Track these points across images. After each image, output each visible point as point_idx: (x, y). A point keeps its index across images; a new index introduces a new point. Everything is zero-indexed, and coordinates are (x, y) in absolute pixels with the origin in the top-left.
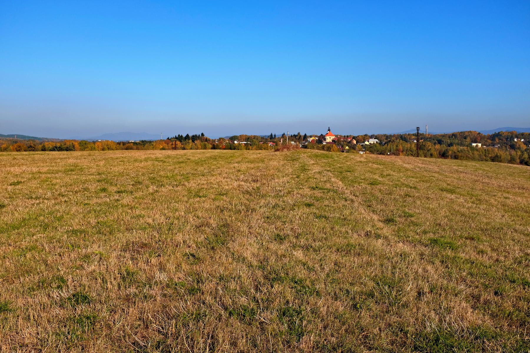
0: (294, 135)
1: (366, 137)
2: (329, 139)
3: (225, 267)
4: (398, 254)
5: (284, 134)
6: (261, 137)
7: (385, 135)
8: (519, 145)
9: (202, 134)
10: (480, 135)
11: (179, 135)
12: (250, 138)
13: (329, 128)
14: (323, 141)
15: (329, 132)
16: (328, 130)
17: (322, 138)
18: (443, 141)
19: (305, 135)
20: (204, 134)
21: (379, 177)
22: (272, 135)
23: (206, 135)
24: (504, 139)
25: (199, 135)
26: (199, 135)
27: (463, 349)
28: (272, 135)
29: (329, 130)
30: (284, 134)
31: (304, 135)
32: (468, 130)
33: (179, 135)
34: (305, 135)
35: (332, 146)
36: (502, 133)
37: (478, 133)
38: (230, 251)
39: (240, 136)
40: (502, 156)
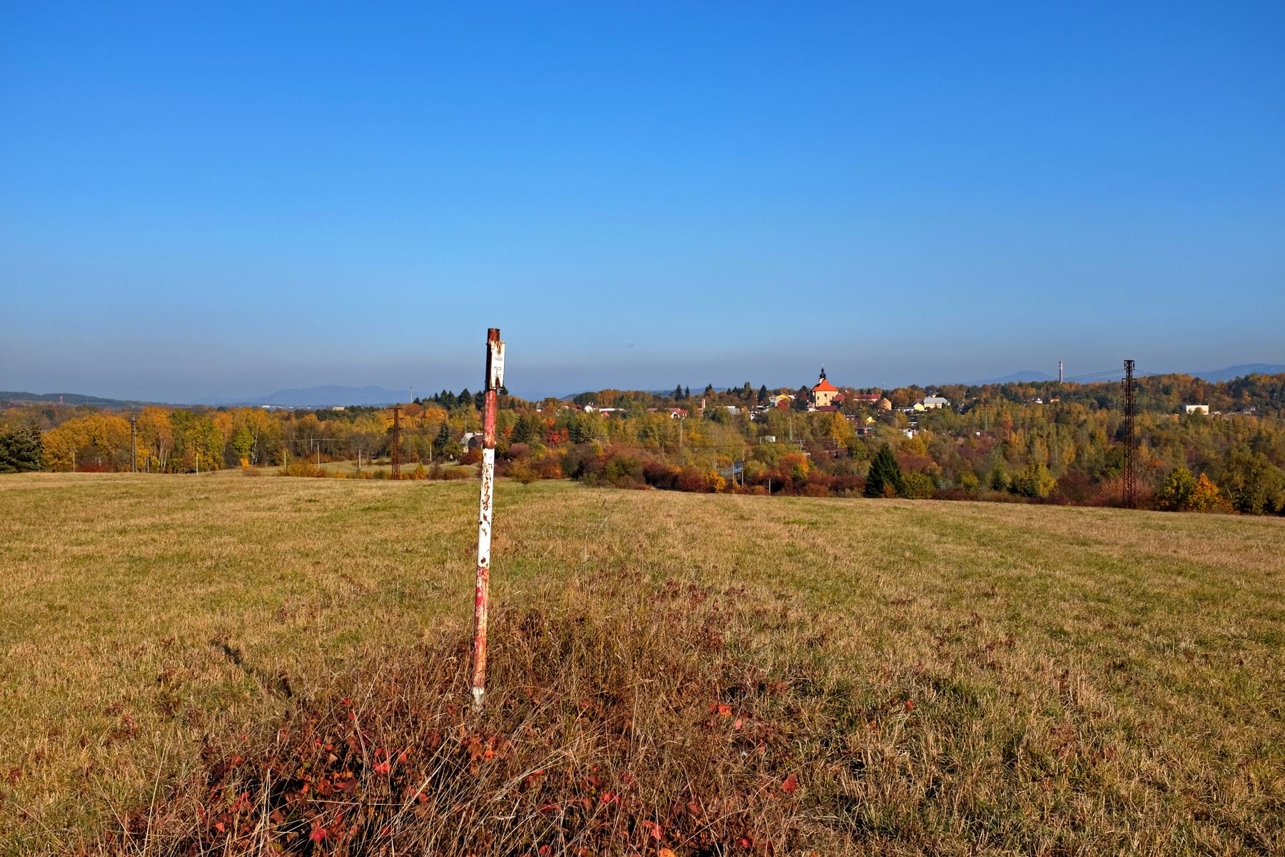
1: (915, 394)
5: (710, 387)
11: (444, 393)
13: (822, 370)
14: (807, 404)
15: (821, 380)
16: (821, 377)
17: (804, 397)
19: (764, 388)
22: (679, 390)
28: (679, 390)
29: (823, 376)
30: (710, 387)
33: (444, 393)
34: (764, 388)
35: (834, 416)
39: (602, 392)
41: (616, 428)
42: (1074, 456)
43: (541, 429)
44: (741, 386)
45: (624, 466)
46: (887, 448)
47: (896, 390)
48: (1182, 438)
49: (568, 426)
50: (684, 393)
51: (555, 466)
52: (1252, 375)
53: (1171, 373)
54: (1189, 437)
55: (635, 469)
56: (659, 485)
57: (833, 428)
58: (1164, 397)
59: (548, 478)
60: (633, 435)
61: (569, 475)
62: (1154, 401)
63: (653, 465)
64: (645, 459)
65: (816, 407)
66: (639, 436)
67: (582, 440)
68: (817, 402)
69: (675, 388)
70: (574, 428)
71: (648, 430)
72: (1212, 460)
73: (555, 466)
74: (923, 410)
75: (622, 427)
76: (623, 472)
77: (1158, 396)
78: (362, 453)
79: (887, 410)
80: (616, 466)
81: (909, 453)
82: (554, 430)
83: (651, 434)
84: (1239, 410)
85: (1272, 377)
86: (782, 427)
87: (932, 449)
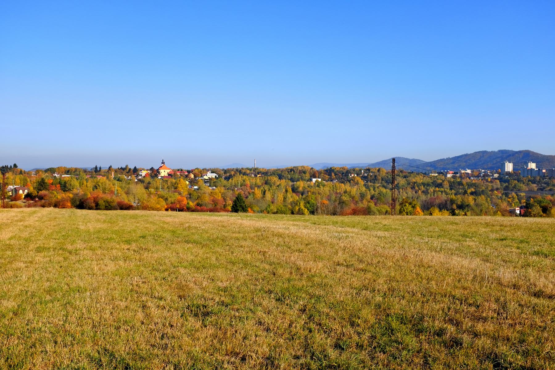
0: (121, 168)
1: (206, 170)
2: (164, 173)
5: (111, 167)
6: (84, 170)
7: (223, 170)
8: (357, 181)
9: (15, 166)
10: (313, 170)
11: (6, 166)
12: (70, 171)
13: (163, 160)
14: (158, 175)
16: (162, 163)
17: (154, 173)
18: (283, 176)
19: (135, 167)
20: (17, 165)
21: (498, 219)
22: (96, 168)
23: (20, 167)
24: (340, 175)
25: (11, 166)
26: (11, 167)
28: (96, 168)
29: (163, 163)
30: (111, 167)
31: (95, 167)
32: (302, 165)
34: (135, 167)
35: (180, 181)
36: (334, 168)
37: (311, 168)
39: (58, 168)
40: (352, 192)
42: (283, 199)
44: (124, 167)
45: (107, 202)
46: (240, 195)
48: (318, 191)
49: (60, 183)
50: (98, 169)
52: (333, 167)
53: (302, 165)
54: (321, 191)
57: (179, 186)
58: (304, 175)
59: (64, 208)
60: (90, 187)
62: (300, 177)
65: (161, 177)
67: (67, 190)
68: (161, 174)
69: (95, 167)
70: (63, 184)
72: (346, 200)
74: (207, 178)
77: (301, 175)
78: (454, 176)
81: (214, 197)
84: (331, 181)
85: (340, 168)
87: (223, 195)
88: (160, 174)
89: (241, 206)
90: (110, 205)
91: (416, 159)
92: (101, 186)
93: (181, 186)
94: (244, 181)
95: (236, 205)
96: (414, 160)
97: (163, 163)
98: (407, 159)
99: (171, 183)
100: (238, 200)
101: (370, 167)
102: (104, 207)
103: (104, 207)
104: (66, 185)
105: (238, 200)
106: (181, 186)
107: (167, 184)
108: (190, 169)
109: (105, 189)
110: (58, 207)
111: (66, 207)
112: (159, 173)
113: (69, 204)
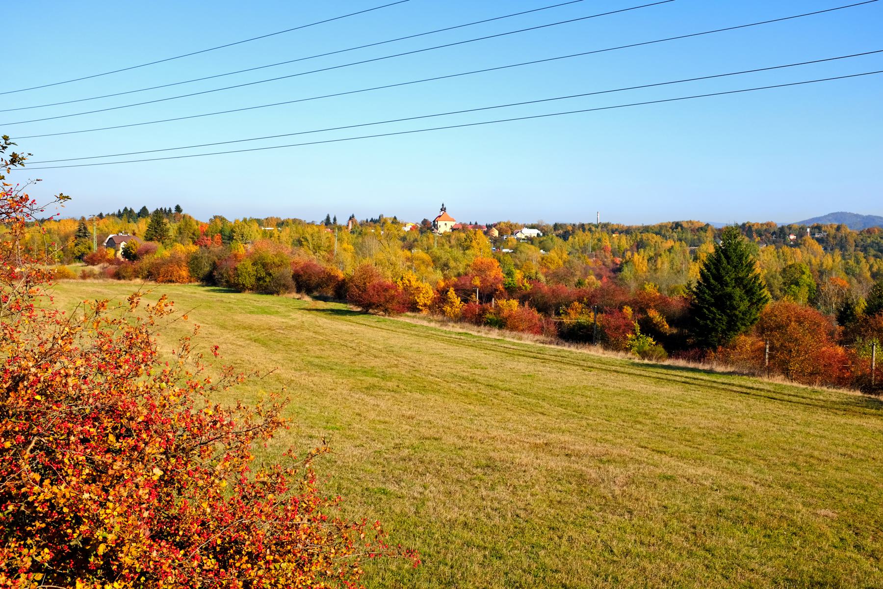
0: (372, 220)
2: (444, 227)
3: (258, 376)
4: (469, 295)
11: (126, 209)
13: (443, 205)
15: (442, 213)
17: (427, 227)
20: (182, 207)
22: (328, 218)
26: (170, 210)
27: (642, 543)
28: (328, 218)
29: (443, 209)
30: (353, 216)
33: (126, 209)
38: (742, 460)
39: (267, 219)
41: (271, 237)
43: (194, 234)
45: (264, 265)
47: (499, 223)
50: (332, 221)
51: (180, 266)
52: (748, 223)
53: (689, 220)
55: (282, 269)
56: (316, 294)
57: (474, 243)
59: (171, 281)
61: (198, 279)
63: (307, 266)
64: (296, 258)
66: (293, 244)
68: (439, 229)
71: (303, 240)
73: (180, 266)
75: (276, 235)
76: (263, 274)
79: (495, 237)
80: (254, 264)
82: (207, 236)
83: (304, 243)
86: (425, 242)
88: (437, 229)
89: (739, 281)
90: (270, 275)
91: (875, 217)
92: (310, 241)
93: (478, 244)
94: (599, 240)
95: (719, 278)
96: (870, 218)
97: (443, 209)
98: (857, 216)
99: (458, 240)
100: (728, 258)
101: (820, 223)
102: (249, 281)
103: (253, 280)
104: (233, 236)
105: (728, 258)
106: (478, 244)
107: (450, 242)
108: (491, 223)
109: (319, 247)
110: (156, 280)
111: (174, 279)
112: (435, 226)
113: (184, 273)
